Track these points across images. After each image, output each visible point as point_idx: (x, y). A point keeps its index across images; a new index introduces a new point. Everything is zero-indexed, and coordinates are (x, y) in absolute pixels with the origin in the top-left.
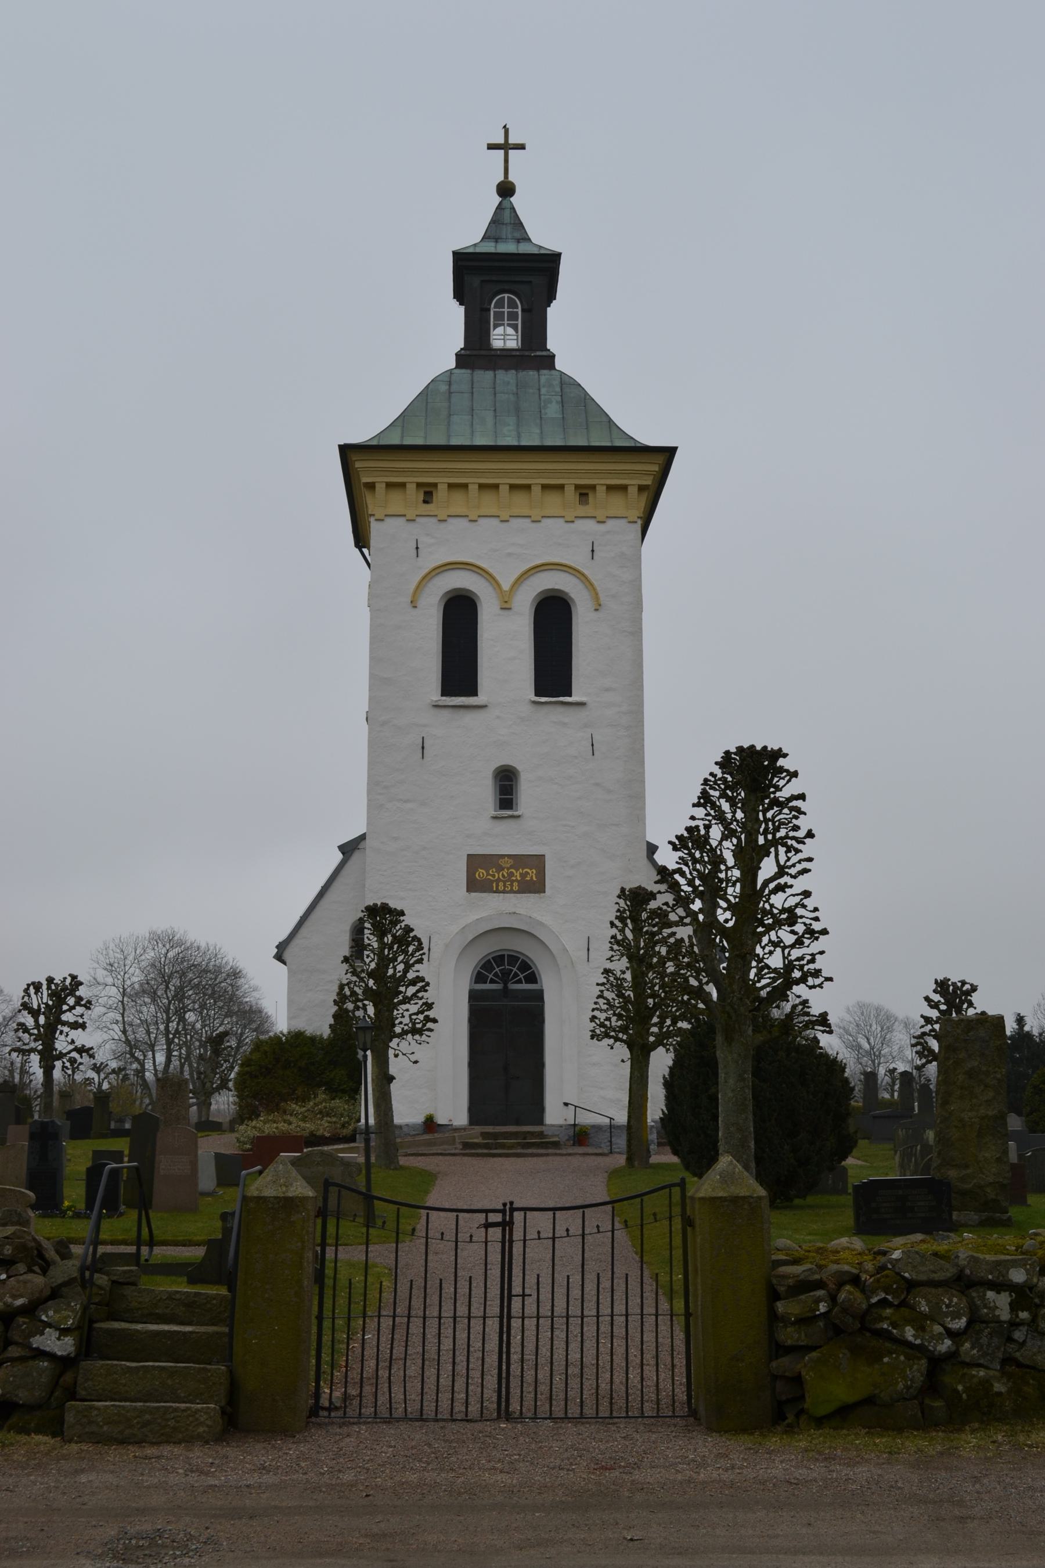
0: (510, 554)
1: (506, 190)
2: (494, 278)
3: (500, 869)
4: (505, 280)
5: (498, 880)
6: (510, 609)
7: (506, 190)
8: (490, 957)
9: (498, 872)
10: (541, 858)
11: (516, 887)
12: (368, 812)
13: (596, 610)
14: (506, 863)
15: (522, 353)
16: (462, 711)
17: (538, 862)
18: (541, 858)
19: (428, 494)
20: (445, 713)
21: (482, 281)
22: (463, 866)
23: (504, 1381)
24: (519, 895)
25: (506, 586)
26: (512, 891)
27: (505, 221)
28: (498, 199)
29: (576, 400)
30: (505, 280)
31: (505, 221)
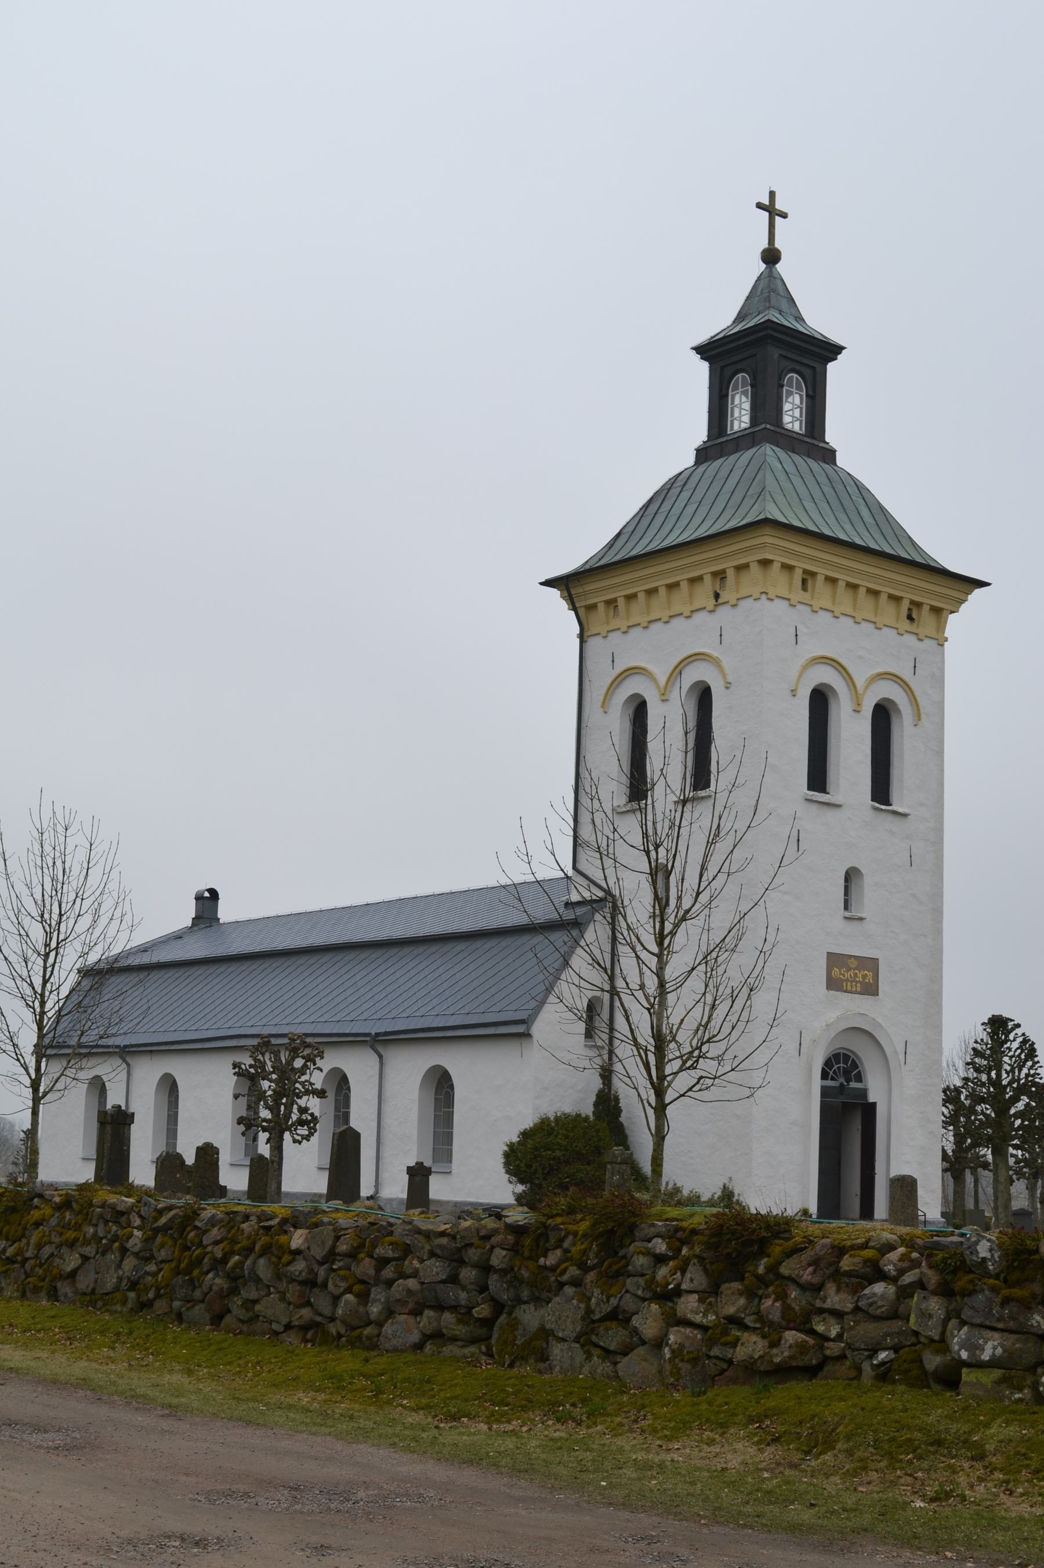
0: (860, 657)
1: (771, 257)
2: (789, 355)
3: (849, 969)
4: (768, 358)
5: (847, 980)
6: (858, 712)
7: (771, 257)
8: (842, 1051)
9: (847, 972)
10: (876, 961)
11: (859, 989)
12: (942, 945)
13: (727, 688)
14: (853, 963)
15: (751, 430)
16: (825, 808)
17: (872, 964)
18: (876, 961)
19: (808, 577)
20: (814, 807)
21: (781, 355)
22: (823, 962)
23: (105, 1050)
24: (862, 996)
25: (860, 683)
26: (856, 992)
27: (769, 288)
28: (763, 266)
29: (856, 496)
30: (768, 358)
31: (769, 288)
